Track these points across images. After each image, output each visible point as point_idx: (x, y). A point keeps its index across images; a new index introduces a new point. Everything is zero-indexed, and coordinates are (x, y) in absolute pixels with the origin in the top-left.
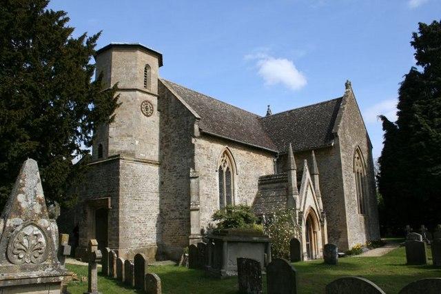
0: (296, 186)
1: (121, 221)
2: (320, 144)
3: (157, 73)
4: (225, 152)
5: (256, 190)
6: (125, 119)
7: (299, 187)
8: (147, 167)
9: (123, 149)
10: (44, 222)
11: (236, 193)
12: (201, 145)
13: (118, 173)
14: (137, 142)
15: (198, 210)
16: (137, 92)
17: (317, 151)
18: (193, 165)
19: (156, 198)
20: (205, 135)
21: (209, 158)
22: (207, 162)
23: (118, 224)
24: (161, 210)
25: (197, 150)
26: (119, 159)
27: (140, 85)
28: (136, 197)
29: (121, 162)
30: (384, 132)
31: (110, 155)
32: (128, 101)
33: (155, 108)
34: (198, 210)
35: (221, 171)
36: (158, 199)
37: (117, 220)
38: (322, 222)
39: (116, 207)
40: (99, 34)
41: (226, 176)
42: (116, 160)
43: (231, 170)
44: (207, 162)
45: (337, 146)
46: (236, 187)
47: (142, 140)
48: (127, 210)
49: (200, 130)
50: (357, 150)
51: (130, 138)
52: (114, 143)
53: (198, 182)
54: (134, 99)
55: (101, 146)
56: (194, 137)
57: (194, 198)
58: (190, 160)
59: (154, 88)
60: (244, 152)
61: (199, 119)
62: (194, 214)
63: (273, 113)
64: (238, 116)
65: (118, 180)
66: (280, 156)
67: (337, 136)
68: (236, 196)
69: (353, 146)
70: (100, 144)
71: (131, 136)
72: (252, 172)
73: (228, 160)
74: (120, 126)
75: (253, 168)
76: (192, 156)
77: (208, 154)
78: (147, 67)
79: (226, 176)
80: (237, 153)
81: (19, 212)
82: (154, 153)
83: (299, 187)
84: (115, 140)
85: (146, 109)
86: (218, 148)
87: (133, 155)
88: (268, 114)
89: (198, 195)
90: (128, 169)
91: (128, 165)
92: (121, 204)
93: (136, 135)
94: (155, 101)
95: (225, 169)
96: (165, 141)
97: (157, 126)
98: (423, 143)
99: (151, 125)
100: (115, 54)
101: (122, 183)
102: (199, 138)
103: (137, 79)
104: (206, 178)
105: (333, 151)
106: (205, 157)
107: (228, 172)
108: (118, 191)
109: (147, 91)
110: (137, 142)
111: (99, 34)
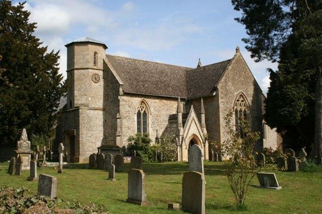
0: (181, 122)
1: (80, 142)
2: (206, 94)
3: (102, 54)
4: (142, 102)
5: (166, 123)
6: (83, 86)
7: (184, 123)
8: (96, 112)
9: (82, 103)
10: (27, 141)
11: (150, 126)
12: (123, 99)
13: (79, 117)
14: (90, 99)
15: (120, 136)
16: (89, 70)
17: (205, 98)
18: (118, 111)
19: (101, 129)
20: (126, 94)
21: (129, 107)
22: (128, 109)
23: (79, 143)
24: (104, 135)
25: (121, 103)
26: (79, 109)
27: (91, 65)
28: (90, 129)
29: (80, 110)
30: (270, 81)
31: (75, 106)
32: (84, 75)
33: (101, 77)
34: (120, 136)
35: (139, 114)
36: (103, 129)
37: (78, 141)
38: (204, 143)
39: (78, 134)
40: (59, 51)
41: (142, 118)
42: (78, 109)
43: (147, 112)
44: (128, 109)
45: (217, 95)
46: (150, 121)
47: (93, 97)
48: (84, 136)
49: (123, 91)
50: (241, 95)
51: (86, 97)
52: (77, 100)
53: (121, 121)
54: (88, 74)
55: (71, 100)
56: (120, 95)
57: (119, 129)
58: (118, 108)
59: (100, 65)
60: (157, 101)
61: (122, 85)
62: (118, 138)
63: (203, 65)
64: (164, 71)
65: (79, 120)
66: (188, 101)
67: (218, 89)
68: (150, 128)
69: (236, 93)
70: (71, 101)
71: (86, 95)
72: (164, 112)
73: (145, 106)
74: (81, 89)
75: (160, 112)
76: (119, 106)
77: (129, 106)
78: (95, 53)
79: (142, 118)
80: (151, 102)
81: (22, 140)
82: (100, 103)
83: (184, 123)
84: (78, 98)
85: (96, 79)
86: (137, 100)
87: (87, 106)
88: (199, 66)
89: (121, 128)
90: (84, 114)
91: (84, 112)
92: (80, 133)
93: (90, 96)
94: (101, 73)
95: (142, 112)
96: (106, 96)
97: (102, 87)
98: (278, 92)
99: (99, 88)
100: (76, 47)
101: (81, 121)
102: (122, 95)
103: (89, 62)
104: (127, 118)
105: (215, 98)
106: (127, 106)
107: (145, 113)
108: (79, 126)
109: (96, 68)
110: (90, 99)
111: (59, 51)
